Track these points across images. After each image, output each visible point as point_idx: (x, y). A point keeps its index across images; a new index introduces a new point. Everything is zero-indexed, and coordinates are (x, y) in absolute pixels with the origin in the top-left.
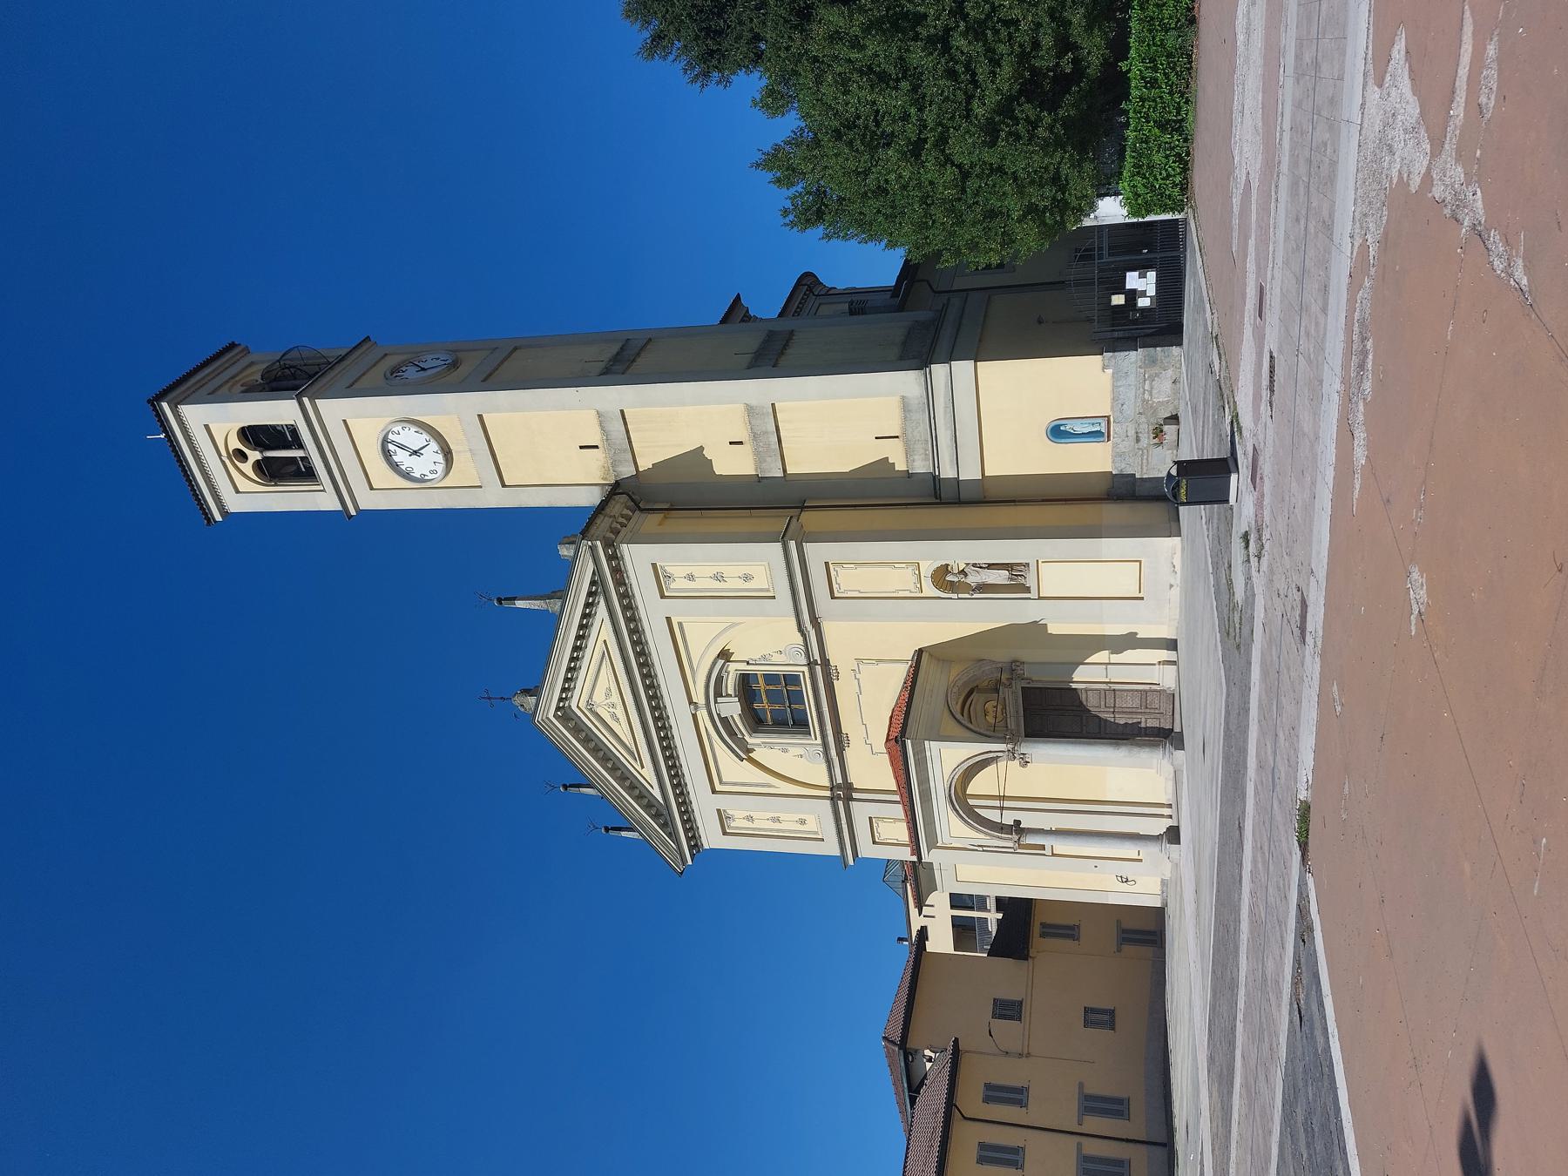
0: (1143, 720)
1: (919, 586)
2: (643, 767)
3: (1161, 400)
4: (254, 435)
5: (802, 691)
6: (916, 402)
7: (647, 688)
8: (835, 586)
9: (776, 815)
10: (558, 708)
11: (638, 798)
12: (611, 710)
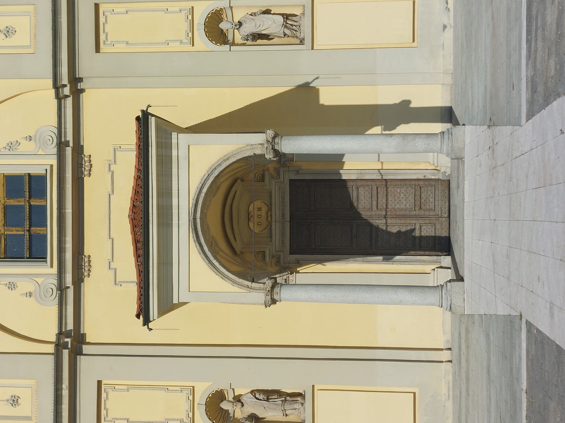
0: (418, 227)
1: (191, 415)
5: (46, 236)
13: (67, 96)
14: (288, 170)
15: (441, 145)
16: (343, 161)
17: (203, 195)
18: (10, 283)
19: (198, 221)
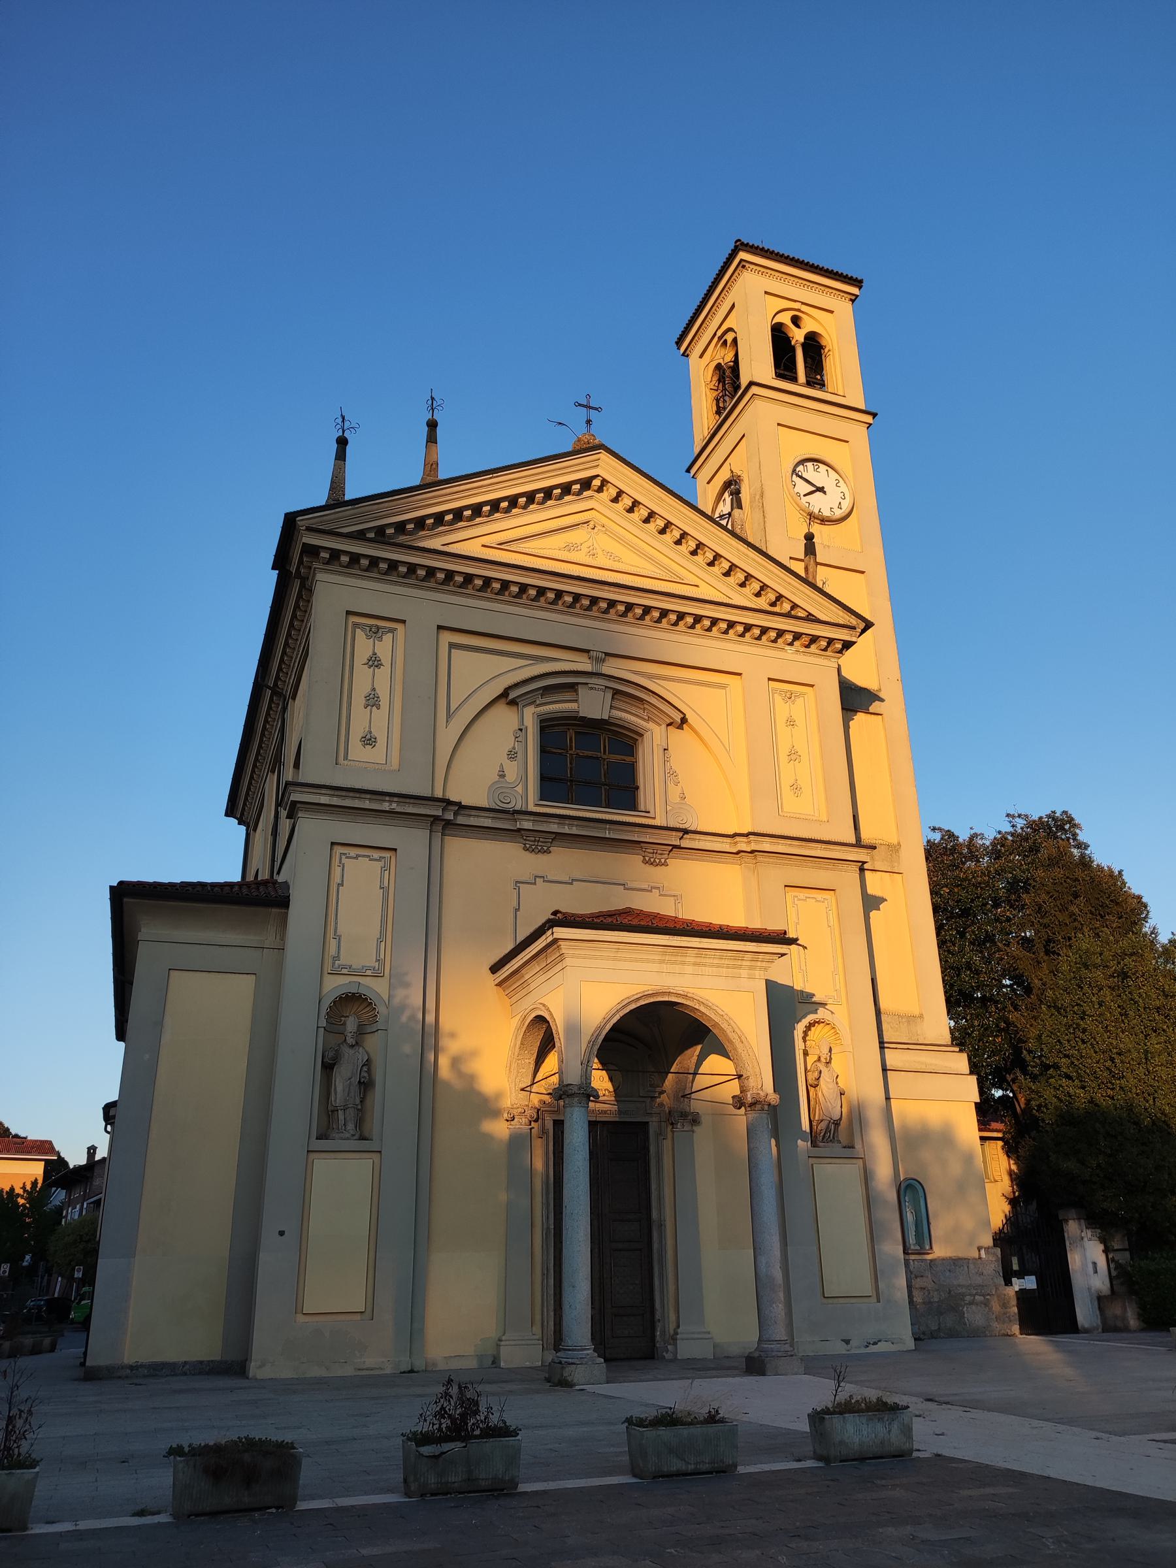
1: (345, 971)
3: (966, 1315)
4: (813, 345)
9: (384, 702)
14: (662, 1120)
15: (776, 1341)
18: (516, 753)
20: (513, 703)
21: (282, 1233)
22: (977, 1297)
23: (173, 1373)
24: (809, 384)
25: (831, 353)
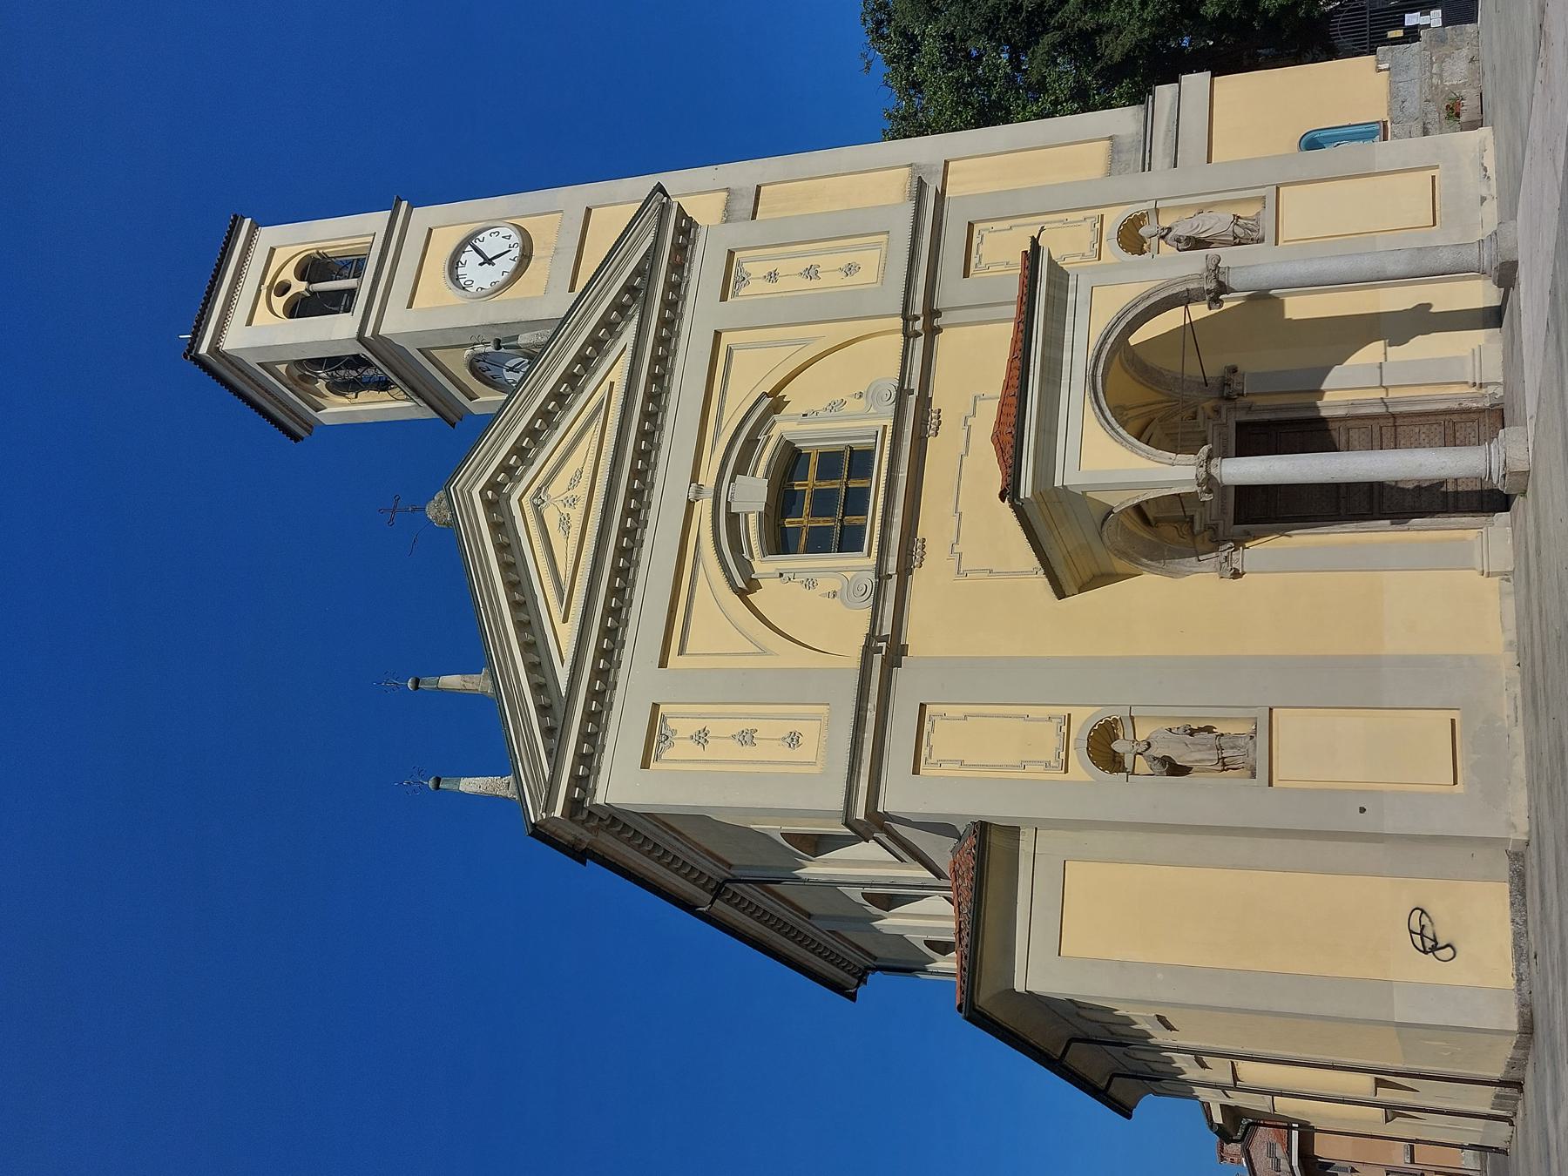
2: (565, 620)
3: (1455, 83)
4: (312, 268)
6: (1130, 140)
7: (623, 532)
8: (974, 260)
9: (849, 280)
10: (493, 485)
11: (532, 668)
12: (567, 510)
13: (918, 335)
16: (1322, 388)
17: (1108, 346)
19: (1099, 380)
20: (753, 585)
21: (1362, 810)
22: (1434, 71)
23: (1525, 935)
24: (358, 273)
25: (321, 251)
